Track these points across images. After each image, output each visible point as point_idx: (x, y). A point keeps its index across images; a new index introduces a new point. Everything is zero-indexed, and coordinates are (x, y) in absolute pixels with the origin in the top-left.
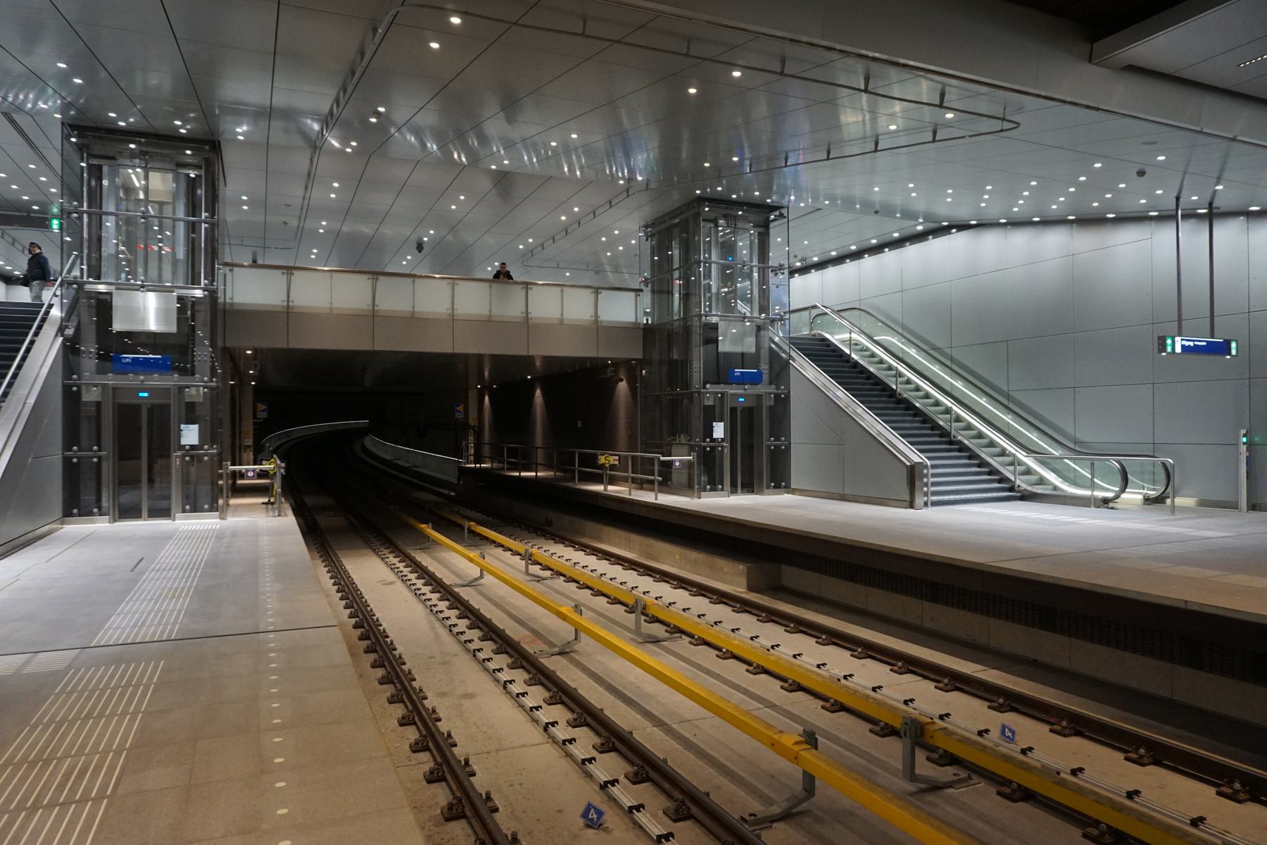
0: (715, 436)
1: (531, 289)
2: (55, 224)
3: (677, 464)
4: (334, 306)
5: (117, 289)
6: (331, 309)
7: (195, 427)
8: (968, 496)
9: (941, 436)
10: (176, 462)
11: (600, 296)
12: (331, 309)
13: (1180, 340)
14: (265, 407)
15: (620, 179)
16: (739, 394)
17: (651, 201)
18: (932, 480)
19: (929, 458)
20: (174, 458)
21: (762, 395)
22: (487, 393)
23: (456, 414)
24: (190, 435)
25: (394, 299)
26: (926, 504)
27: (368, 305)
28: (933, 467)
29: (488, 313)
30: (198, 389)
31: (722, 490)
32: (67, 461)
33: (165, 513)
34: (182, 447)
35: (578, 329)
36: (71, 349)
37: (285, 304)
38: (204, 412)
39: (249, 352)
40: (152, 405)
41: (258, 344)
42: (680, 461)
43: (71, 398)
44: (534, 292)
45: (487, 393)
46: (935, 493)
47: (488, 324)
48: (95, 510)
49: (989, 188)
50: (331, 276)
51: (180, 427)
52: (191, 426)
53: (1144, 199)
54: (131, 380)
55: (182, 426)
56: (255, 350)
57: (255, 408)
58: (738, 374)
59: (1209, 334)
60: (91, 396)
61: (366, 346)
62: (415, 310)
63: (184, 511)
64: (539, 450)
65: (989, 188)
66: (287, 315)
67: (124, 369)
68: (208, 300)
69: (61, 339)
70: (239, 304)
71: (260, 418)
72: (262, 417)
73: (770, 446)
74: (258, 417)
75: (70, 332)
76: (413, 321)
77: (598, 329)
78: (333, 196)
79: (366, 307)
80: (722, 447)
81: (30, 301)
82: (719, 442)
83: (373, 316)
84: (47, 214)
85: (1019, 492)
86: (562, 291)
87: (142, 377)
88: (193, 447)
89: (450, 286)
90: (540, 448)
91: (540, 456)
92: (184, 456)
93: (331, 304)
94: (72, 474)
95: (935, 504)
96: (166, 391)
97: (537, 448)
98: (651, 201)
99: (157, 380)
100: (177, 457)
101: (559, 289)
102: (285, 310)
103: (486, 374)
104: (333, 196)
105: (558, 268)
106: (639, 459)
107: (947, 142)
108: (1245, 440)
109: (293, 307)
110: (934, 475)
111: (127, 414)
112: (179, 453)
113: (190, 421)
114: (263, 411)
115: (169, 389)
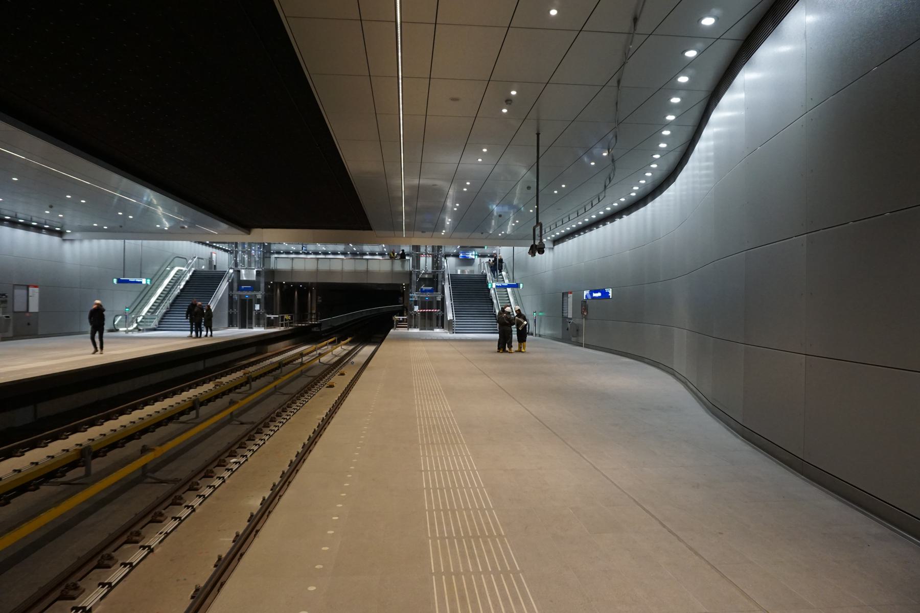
0: (415, 310)
6: (305, 269)
12: (305, 269)
17: (141, 259)
24: (257, 307)
30: (259, 296)
32: (229, 313)
33: (252, 328)
34: (255, 310)
36: (231, 286)
38: (263, 301)
43: (231, 298)
47: (355, 273)
49: (465, 190)
56: (286, 283)
57: (317, 299)
60: (236, 297)
61: (390, 282)
65: (465, 190)
66: (292, 272)
67: (242, 290)
68: (145, 286)
69: (228, 283)
75: (230, 281)
76: (330, 273)
83: (317, 272)
88: (258, 310)
96: (252, 296)
98: (141, 259)
99: (250, 293)
103: (309, 294)
110: (456, 327)
111: (243, 301)
114: (320, 299)
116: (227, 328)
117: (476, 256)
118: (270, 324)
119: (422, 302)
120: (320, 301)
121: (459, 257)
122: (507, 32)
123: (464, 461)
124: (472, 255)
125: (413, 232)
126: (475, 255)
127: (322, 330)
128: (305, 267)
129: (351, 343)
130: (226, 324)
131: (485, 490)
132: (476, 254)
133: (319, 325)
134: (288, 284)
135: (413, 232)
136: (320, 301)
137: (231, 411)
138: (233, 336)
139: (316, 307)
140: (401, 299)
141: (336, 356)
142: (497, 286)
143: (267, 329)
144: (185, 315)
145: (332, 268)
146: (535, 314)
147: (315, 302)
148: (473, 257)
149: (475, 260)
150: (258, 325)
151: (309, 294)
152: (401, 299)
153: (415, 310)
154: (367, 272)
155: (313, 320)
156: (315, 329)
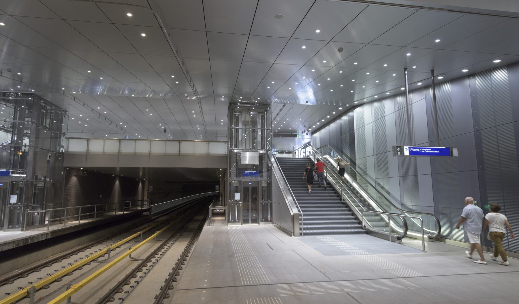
0: (236, 199)
4: (166, 152)
5: (242, 151)
7: (239, 194)
8: (325, 231)
9: (338, 196)
10: (7, 209)
11: (181, 144)
13: (408, 149)
16: (249, 181)
19: (303, 211)
20: (7, 208)
22: (141, 182)
23: (216, 188)
25: (128, 148)
26: (301, 234)
27: (149, 151)
28: (304, 215)
29: (164, 152)
35: (201, 157)
37: (207, 153)
38: (19, 194)
39: (221, 169)
40: (252, 187)
44: (154, 143)
45: (141, 182)
46: (305, 229)
47: (165, 156)
50: (194, 143)
51: (10, 196)
52: (14, 196)
53: (342, 85)
55: (11, 196)
61: (206, 167)
62: (195, 153)
66: (87, 154)
70: (71, 152)
71: (150, 191)
72: (151, 190)
73: (263, 203)
74: (150, 190)
76: (135, 156)
77: (208, 157)
78: (222, 121)
79: (206, 153)
80: (239, 203)
81: (291, 157)
82: (238, 202)
83: (119, 155)
85: (365, 229)
90: (117, 203)
91: (115, 206)
92: (10, 207)
93: (194, 152)
95: (305, 234)
100: (8, 207)
101: (134, 141)
102: (86, 153)
103: (140, 184)
104: (222, 121)
105: (82, 132)
106: (97, 212)
107: (417, 81)
109: (210, 154)
110: (305, 220)
112: (9, 206)
113: (237, 192)
115: (258, 182)
117: (277, 152)
118: (31, 224)
120: (152, 190)
123: (253, 258)
126: (276, 152)
127: (152, 213)
128: (104, 150)
129: (157, 239)
131: (275, 298)
132: (277, 150)
133: (149, 210)
134: (86, 170)
137: (130, 250)
138: (21, 238)
139: (148, 194)
140: (217, 187)
141: (135, 260)
142: (411, 153)
144: (484, 156)
145: (137, 151)
151: (140, 184)
152: (217, 187)
153: (236, 199)
154: (179, 155)
155: (144, 205)
156: (146, 213)
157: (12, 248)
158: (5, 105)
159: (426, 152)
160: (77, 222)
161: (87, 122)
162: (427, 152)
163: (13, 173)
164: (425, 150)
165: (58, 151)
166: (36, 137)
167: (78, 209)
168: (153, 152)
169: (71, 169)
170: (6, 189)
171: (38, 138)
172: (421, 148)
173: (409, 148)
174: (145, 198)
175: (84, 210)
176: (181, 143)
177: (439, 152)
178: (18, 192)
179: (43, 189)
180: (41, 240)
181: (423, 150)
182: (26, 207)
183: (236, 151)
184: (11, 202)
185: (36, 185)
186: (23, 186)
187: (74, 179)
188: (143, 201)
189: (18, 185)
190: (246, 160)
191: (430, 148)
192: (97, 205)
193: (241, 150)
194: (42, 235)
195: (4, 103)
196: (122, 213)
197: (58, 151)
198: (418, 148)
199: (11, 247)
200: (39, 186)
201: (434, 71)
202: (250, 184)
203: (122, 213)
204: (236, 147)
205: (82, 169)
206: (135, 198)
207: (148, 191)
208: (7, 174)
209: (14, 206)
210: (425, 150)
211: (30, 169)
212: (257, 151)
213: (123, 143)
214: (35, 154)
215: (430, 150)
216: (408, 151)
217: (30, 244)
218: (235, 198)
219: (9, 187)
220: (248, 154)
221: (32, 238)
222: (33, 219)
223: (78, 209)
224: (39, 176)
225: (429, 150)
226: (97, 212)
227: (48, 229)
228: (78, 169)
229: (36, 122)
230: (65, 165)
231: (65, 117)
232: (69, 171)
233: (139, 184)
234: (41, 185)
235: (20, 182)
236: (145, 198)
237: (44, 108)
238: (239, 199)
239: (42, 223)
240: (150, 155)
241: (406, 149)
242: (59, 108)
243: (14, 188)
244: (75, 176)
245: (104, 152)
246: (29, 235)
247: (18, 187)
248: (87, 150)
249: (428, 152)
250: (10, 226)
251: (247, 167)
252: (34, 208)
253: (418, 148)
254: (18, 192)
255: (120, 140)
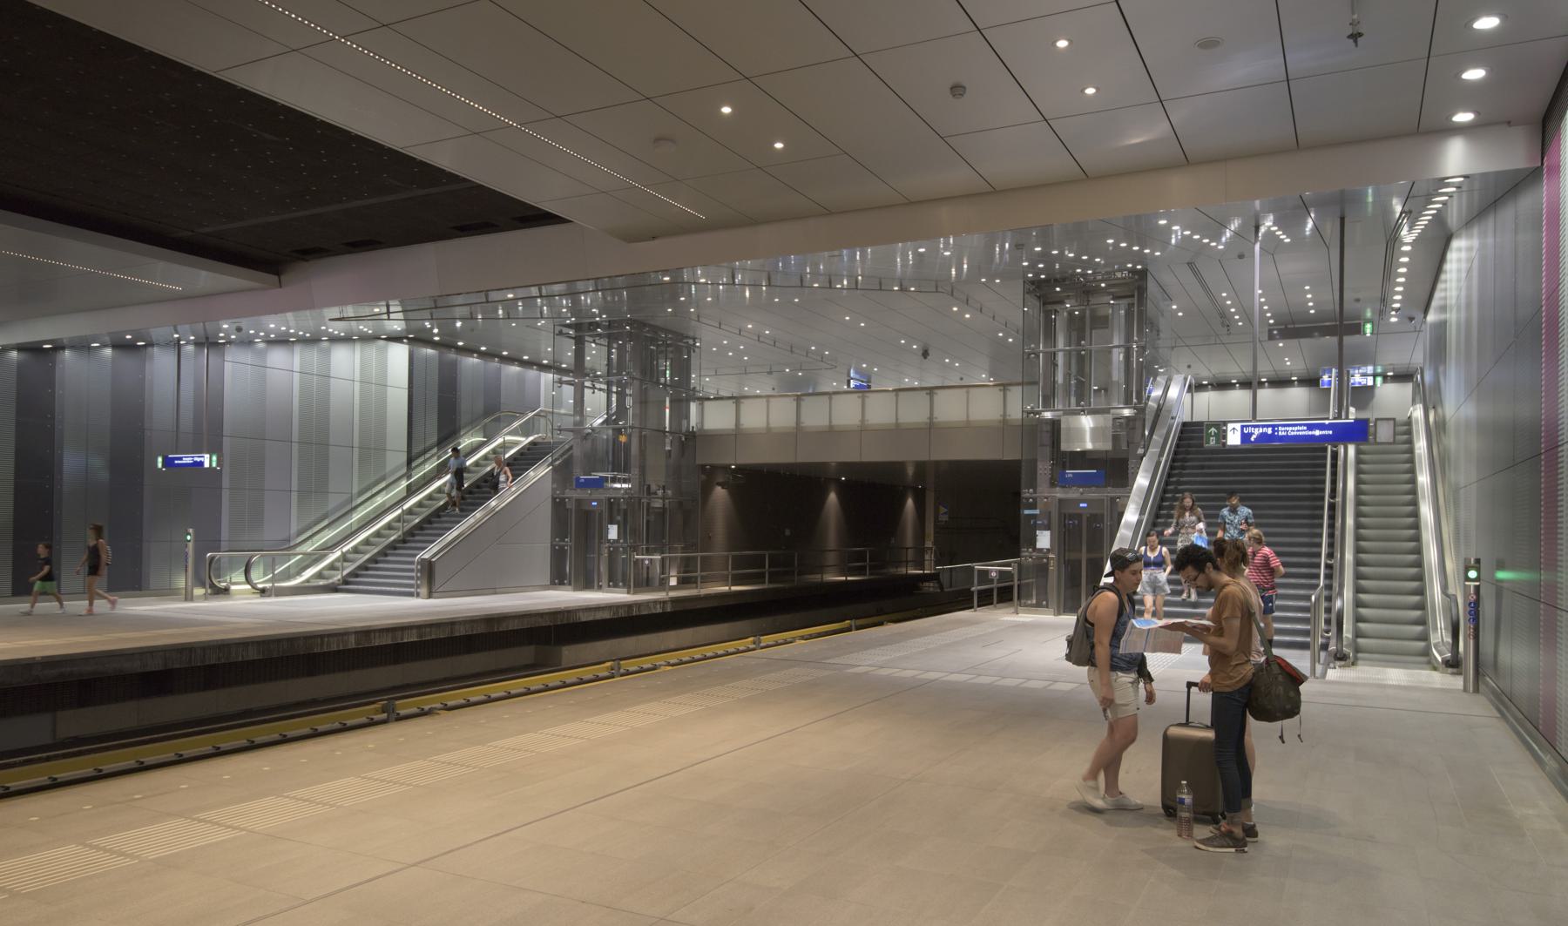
0: (1039, 545)
1: (867, 397)
2: (1368, 327)
3: (994, 574)
4: (900, 421)
5: (1064, 414)
7: (615, 527)
14: (946, 510)
15: (563, 307)
18: (414, 574)
21: (1103, 500)
25: (815, 416)
31: (1047, 606)
40: (1091, 515)
41: (738, 462)
42: (648, 559)
48: (621, 584)
54: (1073, 494)
55: (609, 526)
58: (583, 481)
59: (1035, 387)
63: (609, 586)
64: (910, 550)
66: (738, 435)
67: (1066, 483)
70: (711, 430)
72: (944, 520)
76: (831, 433)
80: (1048, 558)
83: (798, 433)
84: (1359, 319)
86: (968, 392)
87: (1081, 490)
89: (860, 400)
91: (831, 558)
94: (558, 556)
97: (907, 548)
99: (1093, 494)
103: (910, 502)
108: (189, 538)
110: (412, 570)
114: (945, 513)
116: (545, 588)
117: (1379, 380)
118: (644, 583)
119: (1064, 517)
120: (944, 518)
121: (1318, 385)
122: (964, 9)
124: (1364, 375)
125: (332, 380)
126: (1375, 376)
130: (546, 578)
133: (934, 577)
134: (741, 469)
135: (332, 380)
136: (944, 518)
139: (935, 533)
143: (635, 593)
146: (1473, 574)
147: (932, 519)
148: (1370, 381)
149: (1377, 392)
150: (614, 582)
151: (910, 502)
157: (608, 617)
158: (594, 342)
159: (1292, 433)
160: (727, 588)
161: (744, 353)
162: (1295, 433)
163: (614, 480)
164: (1288, 429)
165: (684, 429)
166: (641, 403)
167: (728, 557)
168: (870, 422)
169: (714, 468)
170: (602, 511)
171: (646, 402)
172: (1278, 426)
173: (1242, 427)
174: (929, 544)
175: (738, 563)
176: (936, 394)
177: (1331, 432)
178: (619, 518)
179: (662, 512)
180: (654, 612)
181: (1283, 429)
182: (635, 549)
183: (1048, 415)
184: (609, 538)
185: (648, 504)
186: (625, 507)
187: (720, 493)
188: (920, 551)
189: (619, 505)
190: (1083, 440)
191: (1304, 425)
192: (770, 552)
193: (1061, 413)
194: (655, 602)
195: (591, 339)
196: (844, 578)
197: (684, 429)
198: (1268, 426)
199: (606, 615)
200: (653, 508)
201: (1346, 220)
202: (1081, 505)
203: (844, 578)
204: (1048, 404)
205: (733, 467)
206: (893, 541)
207: (935, 522)
208: (599, 483)
209: (616, 545)
210: (1290, 428)
211: (635, 471)
212: (1109, 413)
213: (808, 403)
214: (642, 439)
215: (1305, 428)
216: (1238, 434)
217: (636, 616)
218: (1038, 544)
219: (605, 508)
220: (1087, 422)
221: (639, 605)
222: (648, 573)
223: (728, 557)
224: (653, 488)
225: (1300, 428)
226: (772, 569)
227: (667, 595)
228: (726, 468)
229: (638, 377)
230: (699, 461)
231: (694, 351)
232: (710, 474)
233: (902, 504)
234: (657, 504)
235: (619, 499)
236: (929, 544)
237: (653, 341)
238: (1048, 547)
239: (663, 584)
240: (863, 430)
241: (1234, 429)
242: (681, 336)
243: (614, 510)
244: (723, 485)
245: (768, 429)
246: (236, 267)
247: (619, 510)
248: (736, 425)
249: (1298, 433)
250: (611, 584)
251: (1083, 458)
252: (648, 552)
253: (1268, 426)
254: (619, 518)
255: (798, 399)
